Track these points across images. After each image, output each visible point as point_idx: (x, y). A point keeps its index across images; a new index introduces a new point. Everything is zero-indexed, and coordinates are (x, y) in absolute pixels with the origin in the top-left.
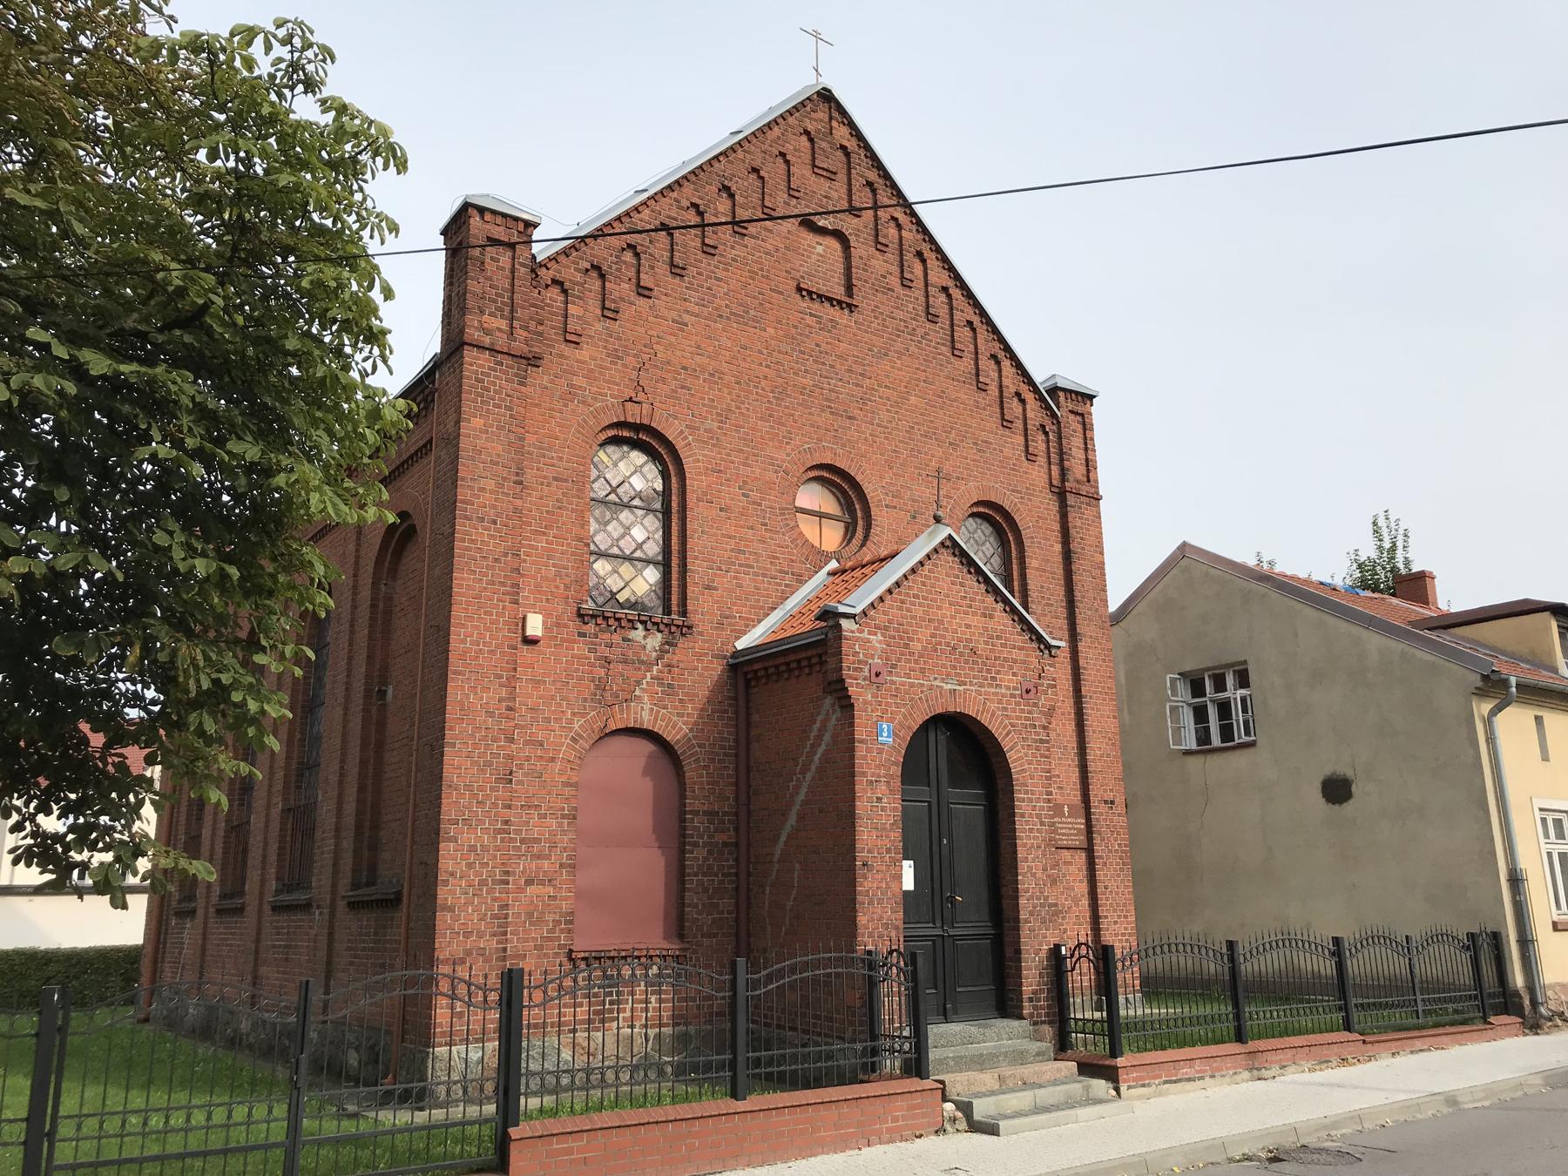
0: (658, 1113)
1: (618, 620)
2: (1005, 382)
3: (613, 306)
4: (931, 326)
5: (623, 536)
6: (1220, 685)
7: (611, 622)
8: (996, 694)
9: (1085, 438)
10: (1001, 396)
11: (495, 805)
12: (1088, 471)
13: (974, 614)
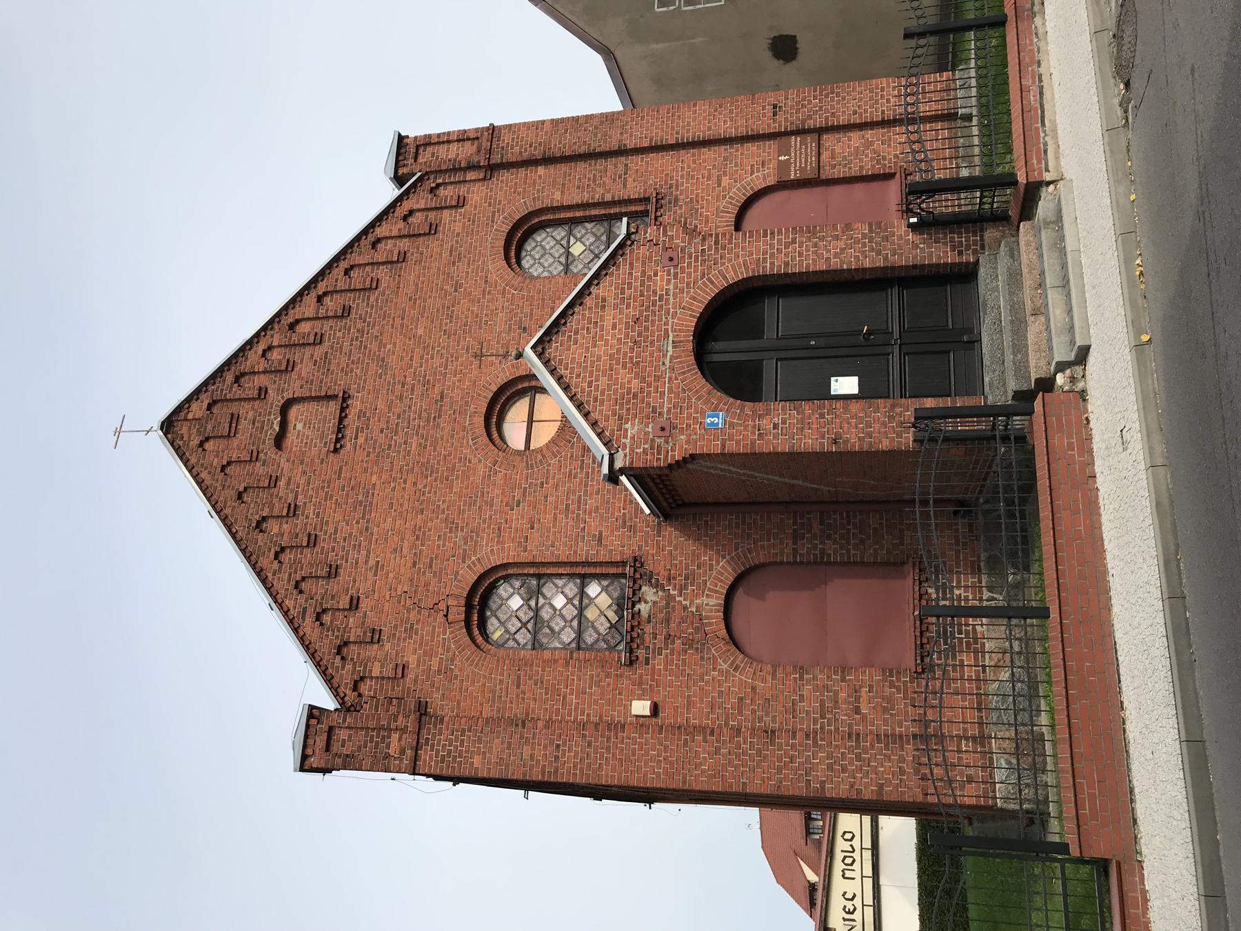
0: (1057, 660)
1: (632, 628)
2: (395, 233)
4: (353, 311)
5: (562, 616)
8: (675, 295)
9: (439, 143)
12: (468, 139)
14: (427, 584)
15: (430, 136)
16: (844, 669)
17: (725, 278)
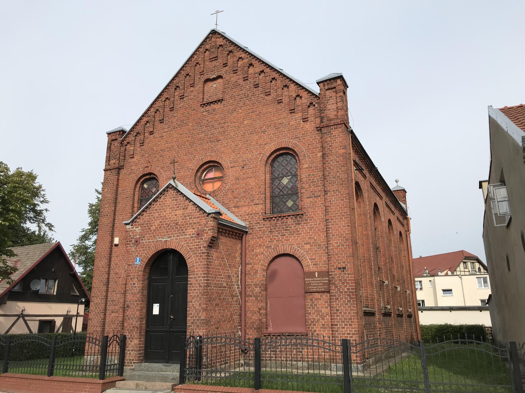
13: (180, 209)
14: (155, 157)
17: (189, 258)
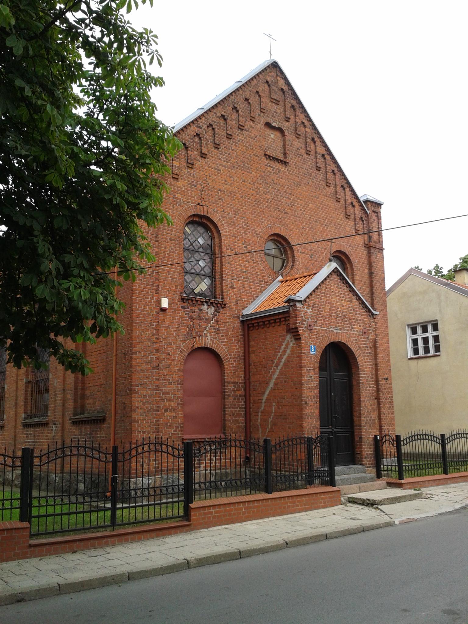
1: (197, 301)
3: (191, 162)
5: (196, 265)
6: (425, 330)
7: (194, 302)
10: (346, 204)
11: (153, 379)
13: (345, 300)
15: (381, 219)
16: (183, 405)
